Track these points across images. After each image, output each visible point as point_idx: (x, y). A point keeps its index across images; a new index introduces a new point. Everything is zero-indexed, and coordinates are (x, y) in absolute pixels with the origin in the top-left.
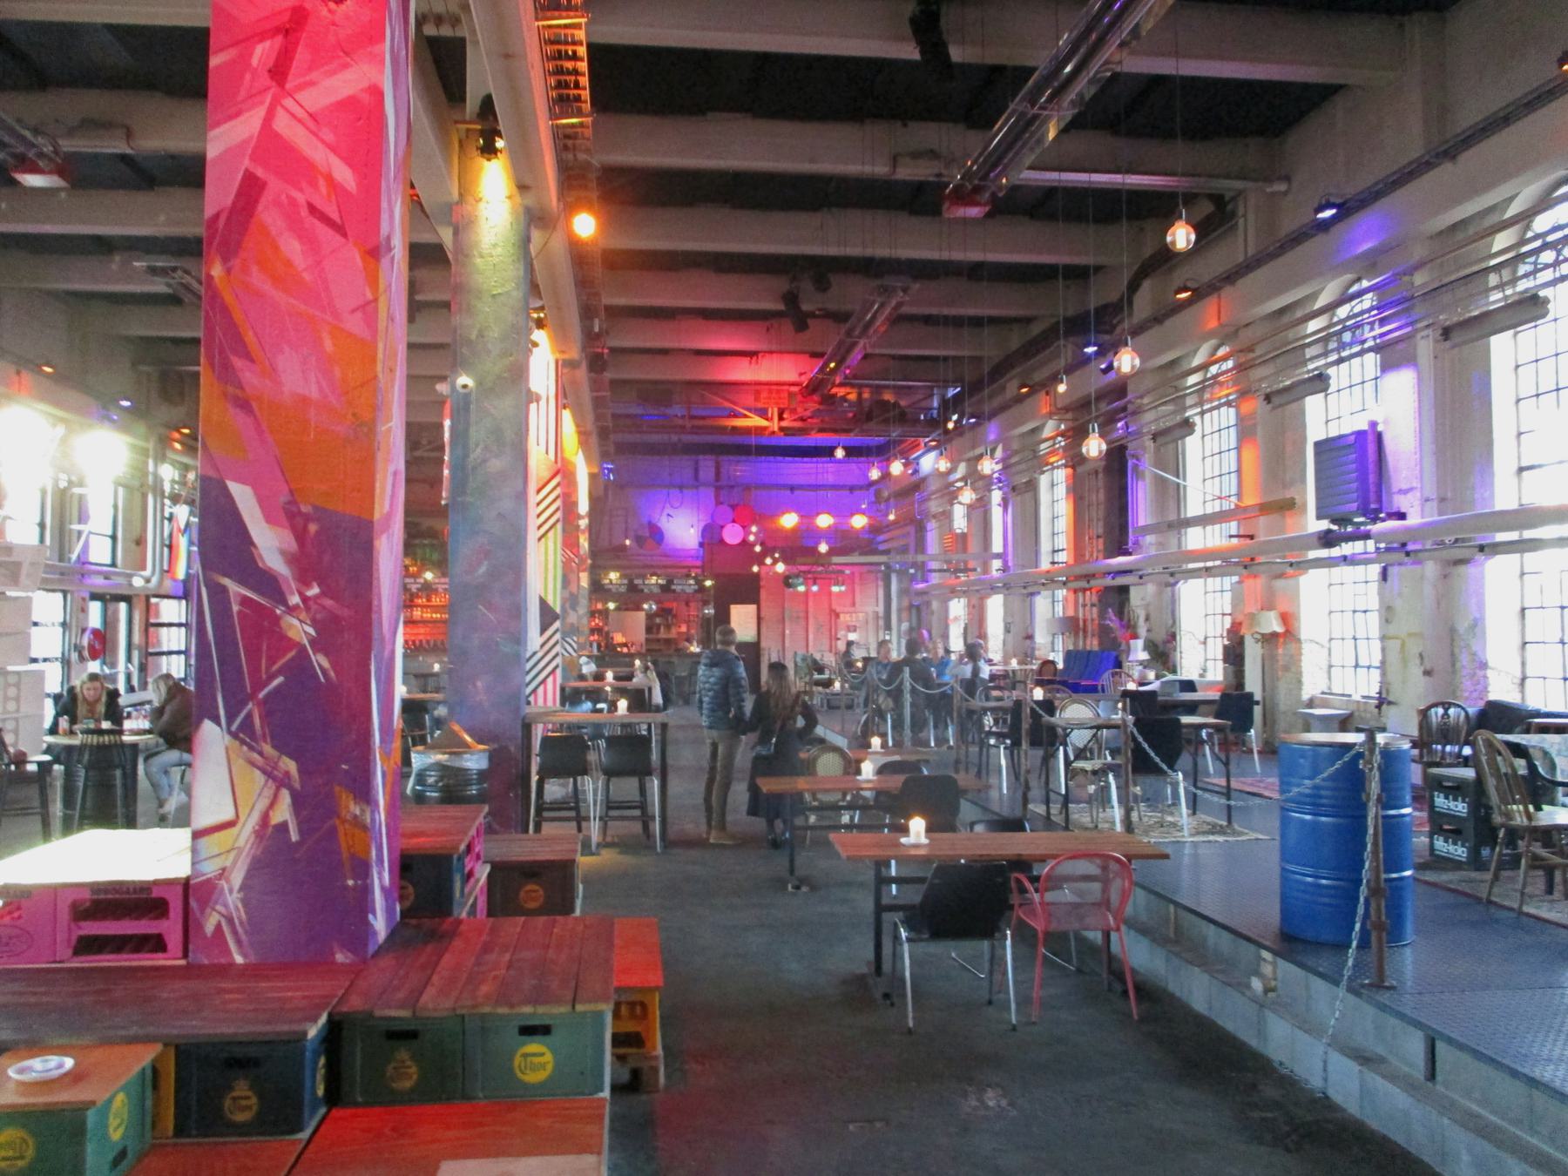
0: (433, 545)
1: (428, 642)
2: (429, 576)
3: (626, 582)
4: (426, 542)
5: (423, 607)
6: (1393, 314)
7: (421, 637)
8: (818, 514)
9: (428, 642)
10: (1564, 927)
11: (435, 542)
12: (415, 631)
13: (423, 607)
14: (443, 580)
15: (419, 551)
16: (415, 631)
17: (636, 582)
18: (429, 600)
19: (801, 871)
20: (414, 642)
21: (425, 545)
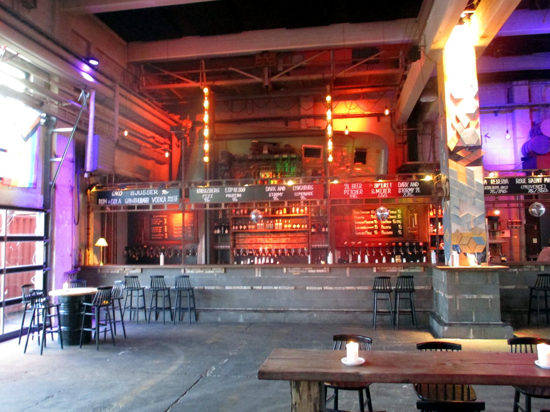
0: (292, 159)
1: (289, 250)
2: (290, 183)
3: (506, 181)
4: (285, 156)
5: (283, 218)
6: (365, 94)
7: (283, 246)
8: (331, 96)
9: (289, 250)
10: (5, 9)
11: (294, 156)
12: (278, 241)
13: (283, 218)
14: (305, 188)
15: (279, 166)
16: (278, 241)
17: (518, 181)
18: (289, 211)
19: (401, 137)
20: (277, 250)
21: (284, 159)
